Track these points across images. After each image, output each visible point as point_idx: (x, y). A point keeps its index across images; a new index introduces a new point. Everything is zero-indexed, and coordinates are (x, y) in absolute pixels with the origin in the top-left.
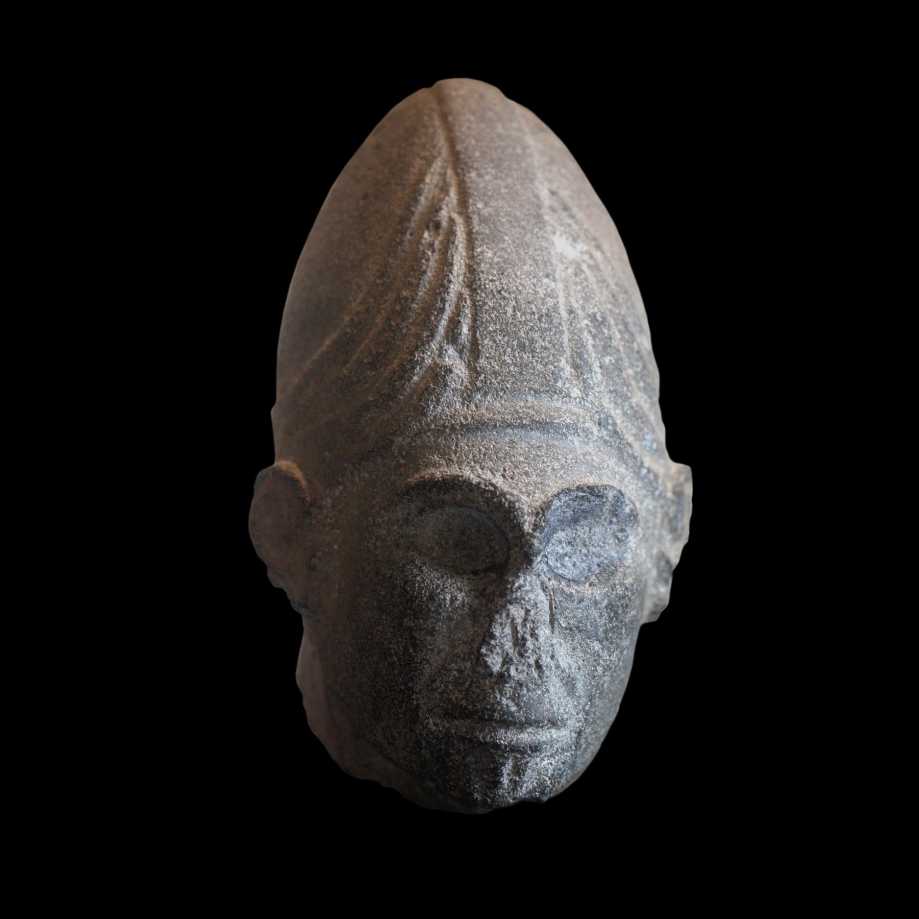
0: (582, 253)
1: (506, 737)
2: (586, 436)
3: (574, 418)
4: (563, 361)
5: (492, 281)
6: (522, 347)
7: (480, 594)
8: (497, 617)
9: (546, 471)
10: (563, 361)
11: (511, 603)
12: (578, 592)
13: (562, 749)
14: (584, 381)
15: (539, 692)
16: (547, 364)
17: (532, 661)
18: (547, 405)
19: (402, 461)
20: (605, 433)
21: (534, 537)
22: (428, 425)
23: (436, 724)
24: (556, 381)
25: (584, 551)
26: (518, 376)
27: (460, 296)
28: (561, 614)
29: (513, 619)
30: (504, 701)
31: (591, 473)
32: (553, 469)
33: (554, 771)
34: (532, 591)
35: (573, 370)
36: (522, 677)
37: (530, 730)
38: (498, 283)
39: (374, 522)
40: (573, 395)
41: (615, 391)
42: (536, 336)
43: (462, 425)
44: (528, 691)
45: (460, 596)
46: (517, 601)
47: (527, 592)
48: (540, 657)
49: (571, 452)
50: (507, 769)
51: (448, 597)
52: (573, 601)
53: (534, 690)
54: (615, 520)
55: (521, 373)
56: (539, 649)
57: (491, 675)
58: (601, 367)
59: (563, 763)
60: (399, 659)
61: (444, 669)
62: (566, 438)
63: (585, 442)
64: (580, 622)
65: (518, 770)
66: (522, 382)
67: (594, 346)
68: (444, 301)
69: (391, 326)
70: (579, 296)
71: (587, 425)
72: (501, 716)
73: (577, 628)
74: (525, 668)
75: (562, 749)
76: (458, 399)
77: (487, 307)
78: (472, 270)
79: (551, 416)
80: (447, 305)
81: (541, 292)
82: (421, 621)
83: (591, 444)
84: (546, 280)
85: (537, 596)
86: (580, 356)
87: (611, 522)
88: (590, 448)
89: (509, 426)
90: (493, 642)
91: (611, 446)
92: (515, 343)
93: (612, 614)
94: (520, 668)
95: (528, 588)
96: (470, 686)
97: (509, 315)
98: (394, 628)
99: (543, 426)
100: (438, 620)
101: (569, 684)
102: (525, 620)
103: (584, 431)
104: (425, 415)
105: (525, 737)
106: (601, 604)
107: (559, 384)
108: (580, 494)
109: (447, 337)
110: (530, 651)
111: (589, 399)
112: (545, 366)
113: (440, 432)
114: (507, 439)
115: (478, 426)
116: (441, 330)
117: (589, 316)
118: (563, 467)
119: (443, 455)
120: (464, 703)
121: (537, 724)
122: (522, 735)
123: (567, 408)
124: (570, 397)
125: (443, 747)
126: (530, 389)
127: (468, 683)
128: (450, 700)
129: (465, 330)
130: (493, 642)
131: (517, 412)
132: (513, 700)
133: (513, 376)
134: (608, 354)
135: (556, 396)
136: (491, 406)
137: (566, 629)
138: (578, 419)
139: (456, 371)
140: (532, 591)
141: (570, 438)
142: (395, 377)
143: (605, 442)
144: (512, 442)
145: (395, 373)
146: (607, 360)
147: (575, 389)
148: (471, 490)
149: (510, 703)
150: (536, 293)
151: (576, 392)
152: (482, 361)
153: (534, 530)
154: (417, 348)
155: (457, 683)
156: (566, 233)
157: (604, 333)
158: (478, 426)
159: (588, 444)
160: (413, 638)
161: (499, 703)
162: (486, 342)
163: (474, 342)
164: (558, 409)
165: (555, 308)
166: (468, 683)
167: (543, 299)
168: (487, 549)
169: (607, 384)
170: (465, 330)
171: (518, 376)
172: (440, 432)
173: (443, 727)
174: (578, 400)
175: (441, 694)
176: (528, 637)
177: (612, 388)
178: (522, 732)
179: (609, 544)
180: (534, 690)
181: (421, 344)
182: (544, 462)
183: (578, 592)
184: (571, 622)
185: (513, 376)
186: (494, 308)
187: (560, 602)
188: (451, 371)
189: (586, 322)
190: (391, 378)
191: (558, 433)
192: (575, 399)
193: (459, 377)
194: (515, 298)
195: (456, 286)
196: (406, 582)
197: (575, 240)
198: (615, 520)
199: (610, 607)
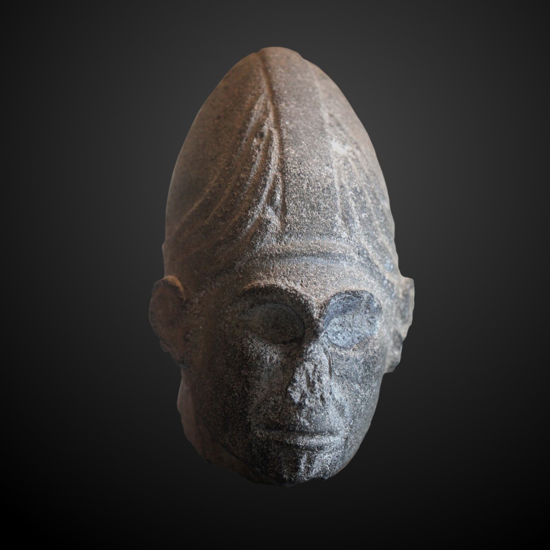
0: (348, 151)
1: (303, 441)
2: (351, 261)
3: (344, 250)
4: (337, 216)
5: (294, 168)
6: (313, 208)
7: (288, 355)
8: (297, 369)
9: (327, 282)
10: (337, 216)
11: (306, 361)
12: (346, 354)
13: (337, 448)
14: (350, 228)
15: (323, 414)
16: (327, 218)
17: (318, 396)
18: (327, 242)
19: (241, 276)
20: (362, 259)
21: (320, 321)
22: (256, 254)
23: (261, 434)
24: (333, 228)
25: (350, 330)
26: (310, 225)
27: (275, 177)
28: (336, 367)
29: (307, 371)
30: (302, 420)
31: (354, 283)
32: (331, 281)
33: (332, 461)
34: (318, 353)
35: (343, 222)
36: (312, 405)
37: (317, 437)
38: (298, 169)
39: (224, 312)
40: (343, 236)
41: (368, 234)
42: (321, 201)
43: (276, 254)
44: (316, 413)
45: (275, 357)
46: (309, 360)
47: (315, 354)
48: (323, 393)
49: (342, 270)
50: (304, 460)
51: (268, 357)
52: (343, 360)
53: (320, 413)
54: (368, 311)
55: (312, 223)
56: (323, 388)
57: (294, 404)
58: (360, 220)
59: (337, 457)
60: (239, 394)
61: (266, 400)
62: (339, 262)
63: (350, 265)
64: (347, 372)
65: (310, 461)
66: (312, 229)
67: (355, 207)
68: (265, 180)
69: (234, 195)
70: (347, 177)
71: (351, 254)
72: (300, 428)
73: (346, 376)
74: (314, 400)
75: (337, 448)
76: (274, 239)
77: (291, 184)
78: (282, 162)
79: (330, 249)
80: (268, 183)
81: (324, 175)
82: (252, 372)
83: (354, 266)
84: (327, 168)
85: (321, 356)
86: (347, 213)
87: (366, 313)
88: (353, 268)
89: (305, 255)
90: (295, 384)
91: (366, 267)
92: (308, 205)
93: (366, 368)
94: (311, 400)
95: (316, 352)
96: (281, 410)
97: (304, 189)
98: (236, 376)
99: (325, 255)
100: (262, 371)
101: (341, 409)
102: (314, 371)
103: (349, 258)
104: (254, 248)
105: (314, 441)
106: (360, 361)
107: (335, 230)
108: (347, 296)
109: (267, 202)
110: (317, 390)
111: (352, 239)
112: (326, 219)
113: (263, 258)
114: (303, 263)
115: (286, 255)
116: (264, 197)
117: (353, 189)
118: (337, 279)
119: (265, 272)
120: (278, 421)
121: (321, 433)
122: (312, 440)
123: (339, 244)
124: (341, 238)
125: (265, 447)
126: (317, 233)
127: (280, 409)
128: (269, 419)
129: (278, 197)
130: (295, 384)
131: (310, 247)
132: (307, 419)
133: (307, 225)
134: (364, 212)
135: (333, 237)
136: (294, 243)
137: (339, 376)
138: (346, 251)
139: (273, 222)
140: (318, 353)
141: (341, 262)
142: (237, 226)
143: (362, 264)
144: (306, 264)
145: (236, 223)
146: (363, 215)
147: (344, 233)
148: (282, 294)
149: (306, 421)
150: (321, 175)
151: (345, 235)
152: (289, 216)
153: (320, 317)
154: (249, 208)
155: (274, 409)
156: (338, 139)
157: (361, 200)
158: (286, 255)
159: (352, 266)
160: (247, 382)
161: (299, 421)
162: (291, 205)
163: (284, 205)
164: (334, 245)
165: (332, 184)
166: (280, 409)
167: (325, 179)
168: (292, 329)
169: (364, 230)
170: (278, 197)
171: (310, 225)
172: (263, 258)
173: (265, 435)
174: (346, 239)
175: (264, 415)
176: (316, 381)
177: (366, 232)
178: (312, 438)
179: (364, 326)
180: (320, 413)
181: (252, 206)
182: (325, 277)
183: (346, 354)
184: (342, 372)
185: (307, 225)
186: (296, 185)
187: (335, 360)
188: (270, 222)
189: (351, 192)
190: (234, 226)
191: (334, 259)
192: (344, 239)
193: (275, 226)
194: (308, 179)
195: (273, 171)
196: (243, 348)
197: (344, 144)
198: (368, 311)
199: (365, 363)
